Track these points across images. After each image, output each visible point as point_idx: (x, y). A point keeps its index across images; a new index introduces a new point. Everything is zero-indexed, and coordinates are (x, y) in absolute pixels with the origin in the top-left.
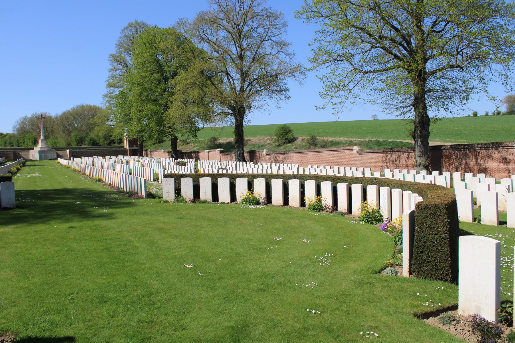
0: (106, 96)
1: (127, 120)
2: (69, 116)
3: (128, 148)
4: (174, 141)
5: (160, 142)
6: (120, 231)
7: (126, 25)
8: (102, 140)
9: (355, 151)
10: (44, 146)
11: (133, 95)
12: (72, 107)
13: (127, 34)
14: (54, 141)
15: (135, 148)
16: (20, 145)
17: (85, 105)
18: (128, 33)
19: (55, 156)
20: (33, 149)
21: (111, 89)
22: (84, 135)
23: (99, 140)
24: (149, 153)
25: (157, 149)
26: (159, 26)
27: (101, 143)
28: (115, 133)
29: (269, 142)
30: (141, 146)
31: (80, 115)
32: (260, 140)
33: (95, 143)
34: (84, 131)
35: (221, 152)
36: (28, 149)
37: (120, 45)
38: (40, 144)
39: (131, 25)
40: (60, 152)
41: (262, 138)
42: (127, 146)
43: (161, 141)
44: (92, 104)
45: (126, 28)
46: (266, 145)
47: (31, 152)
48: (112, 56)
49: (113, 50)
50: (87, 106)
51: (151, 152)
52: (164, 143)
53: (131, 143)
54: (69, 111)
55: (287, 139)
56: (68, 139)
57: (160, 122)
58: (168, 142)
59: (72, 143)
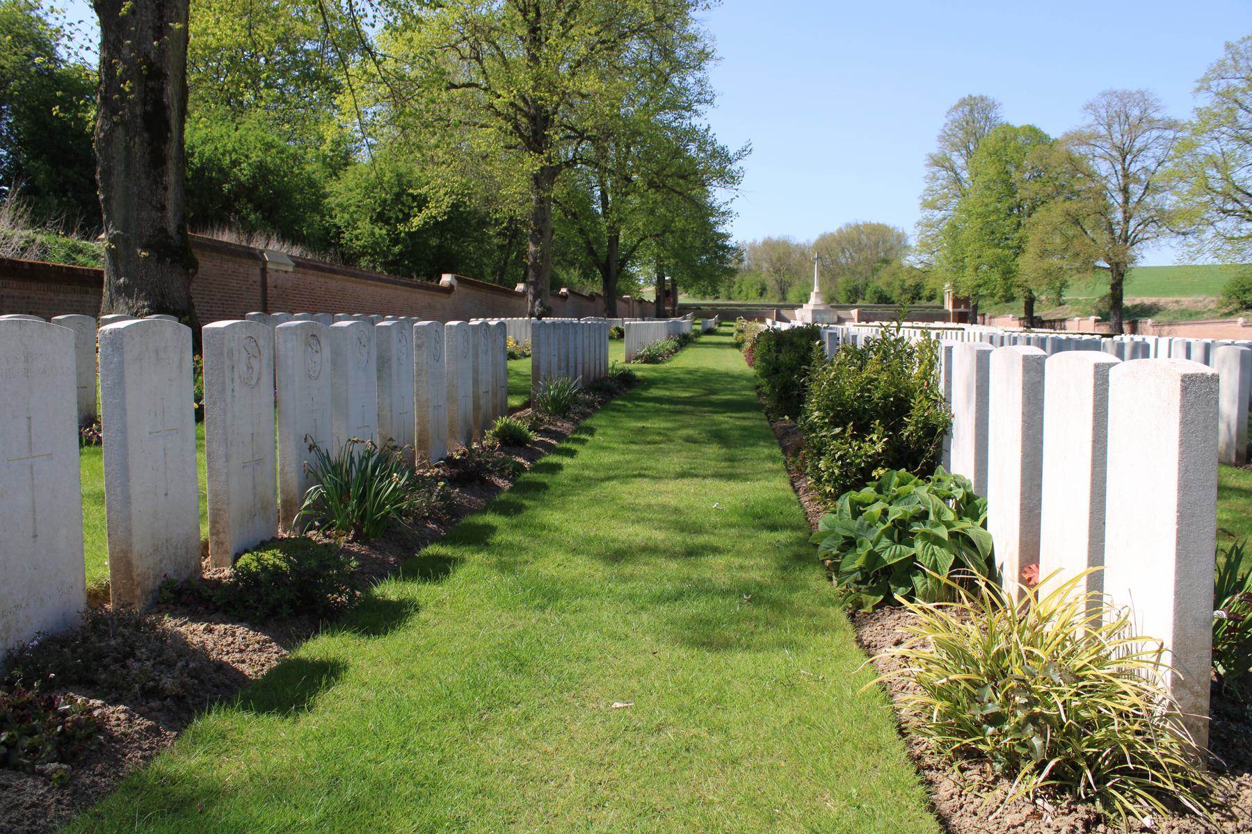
0: (919, 224)
1: (958, 265)
2: (834, 245)
3: (951, 310)
4: (1030, 303)
5: (1007, 301)
6: (659, 807)
7: (955, 102)
8: (898, 291)
9: (1239, 324)
10: (819, 302)
11: (970, 229)
12: (838, 227)
13: (957, 117)
14: (802, 292)
15: (962, 309)
16: (733, 296)
17: (860, 223)
18: (958, 115)
19: (836, 319)
20: (802, 307)
21: (928, 212)
22: (861, 281)
23: (892, 292)
24: (987, 321)
25: (1001, 313)
26: (1011, 123)
27: (895, 299)
28: (930, 284)
29: (1212, 306)
30: (976, 308)
31: (851, 242)
32: (1197, 302)
33: (883, 299)
34: (860, 273)
35: (1096, 321)
36: (793, 307)
37: (942, 139)
38: (813, 299)
39: (963, 103)
40: (842, 313)
41: (1201, 299)
42: (949, 306)
43: (1010, 299)
44: (874, 221)
45: (955, 108)
46: (1204, 313)
47: (797, 312)
48: (931, 156)
49: (934, 148)
50: (866, 225)
51: (990, 318)
52: (1015, 303)
53: (957, 302)
54: (832, 234)
55: (1245, 302)
56: (830, 288)
57: (1008, 273)
58: (1021, 303)
59: (837, 296)
